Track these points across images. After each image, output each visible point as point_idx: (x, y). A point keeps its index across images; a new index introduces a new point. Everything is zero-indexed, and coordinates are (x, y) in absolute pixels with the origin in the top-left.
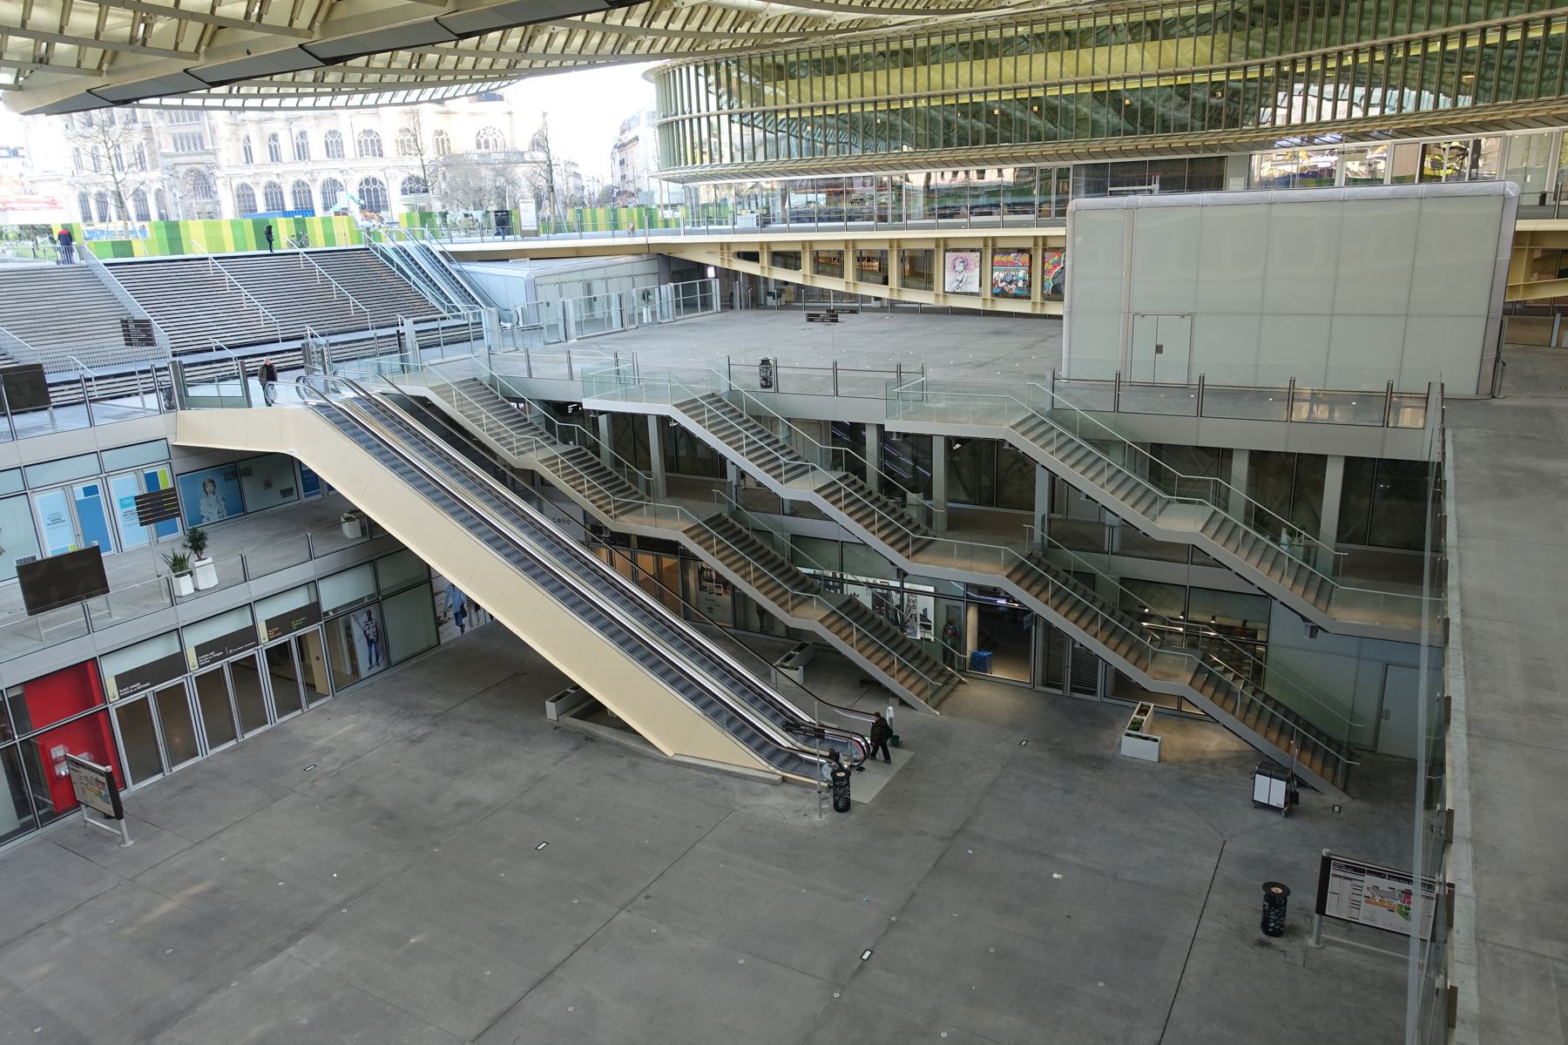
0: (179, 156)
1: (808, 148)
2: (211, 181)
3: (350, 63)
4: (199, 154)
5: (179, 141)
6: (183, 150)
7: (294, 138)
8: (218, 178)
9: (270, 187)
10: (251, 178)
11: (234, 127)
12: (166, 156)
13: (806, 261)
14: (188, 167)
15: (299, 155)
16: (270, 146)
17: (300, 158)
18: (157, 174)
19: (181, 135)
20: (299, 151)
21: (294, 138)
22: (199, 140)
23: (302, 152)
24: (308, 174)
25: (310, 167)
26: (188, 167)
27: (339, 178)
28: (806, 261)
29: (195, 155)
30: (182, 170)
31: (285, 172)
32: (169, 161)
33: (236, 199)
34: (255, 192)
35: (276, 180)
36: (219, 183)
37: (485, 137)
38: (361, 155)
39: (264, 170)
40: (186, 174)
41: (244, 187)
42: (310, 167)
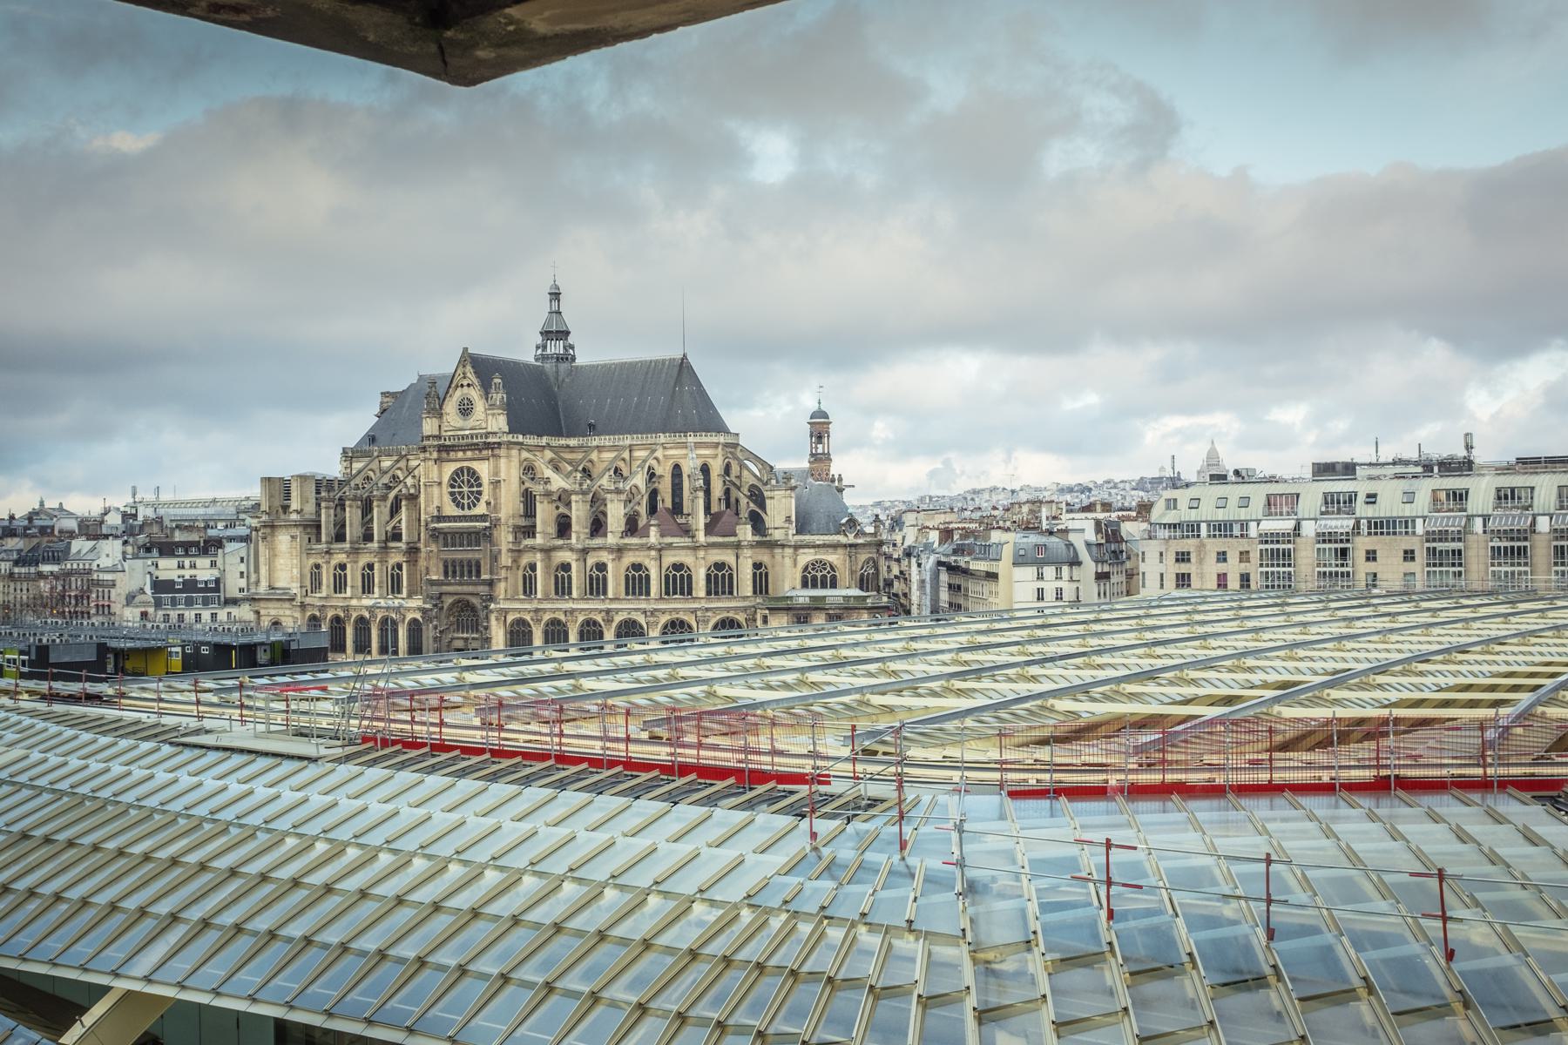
0: (449, 584)
1: (656, 679)
2: (482, 614)
3: (701, 494)
4: (475, 584)
5: (450, 568)
6: (470, 576)
7: (588, 569)
8: (491, 611)
9: (518, 624)
10: (532, 614)
11: (516, 554)
12: (432, 583)
13: (1099, 507)
14: (456, 597)
15: (591, 588)
16: (556, 577)
17: (591, 594)
18: (416, 602)
19: (454, 561)
20: (591, 584)
21: (588, 569)
22: (474, 568)
23: (596, 586)
24: (603, 614)
25: (570, 605)
26: (456, 597)
27: (641, 619)
28: (1099, 507)
29: (468, 584)
30: (449, 601)
31: (656, 610)
32: (435, 590)
33: (508, 636)
34: (534, 629)
35: (562, 618)
36: (493, 617)
37: (813, 573)
38: (667, 593)
39: (549, 606)
40: (453, 604)
41: (521, 622)
42: (570, 605)
